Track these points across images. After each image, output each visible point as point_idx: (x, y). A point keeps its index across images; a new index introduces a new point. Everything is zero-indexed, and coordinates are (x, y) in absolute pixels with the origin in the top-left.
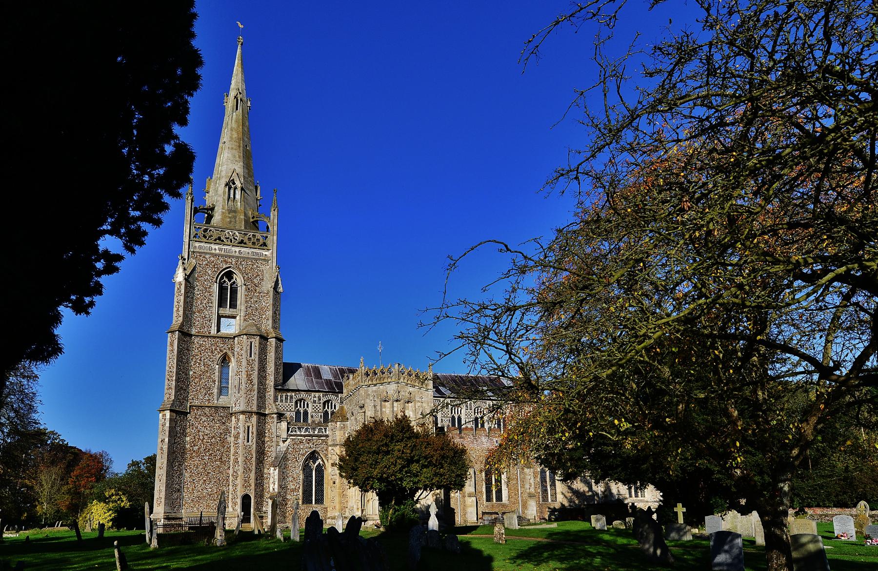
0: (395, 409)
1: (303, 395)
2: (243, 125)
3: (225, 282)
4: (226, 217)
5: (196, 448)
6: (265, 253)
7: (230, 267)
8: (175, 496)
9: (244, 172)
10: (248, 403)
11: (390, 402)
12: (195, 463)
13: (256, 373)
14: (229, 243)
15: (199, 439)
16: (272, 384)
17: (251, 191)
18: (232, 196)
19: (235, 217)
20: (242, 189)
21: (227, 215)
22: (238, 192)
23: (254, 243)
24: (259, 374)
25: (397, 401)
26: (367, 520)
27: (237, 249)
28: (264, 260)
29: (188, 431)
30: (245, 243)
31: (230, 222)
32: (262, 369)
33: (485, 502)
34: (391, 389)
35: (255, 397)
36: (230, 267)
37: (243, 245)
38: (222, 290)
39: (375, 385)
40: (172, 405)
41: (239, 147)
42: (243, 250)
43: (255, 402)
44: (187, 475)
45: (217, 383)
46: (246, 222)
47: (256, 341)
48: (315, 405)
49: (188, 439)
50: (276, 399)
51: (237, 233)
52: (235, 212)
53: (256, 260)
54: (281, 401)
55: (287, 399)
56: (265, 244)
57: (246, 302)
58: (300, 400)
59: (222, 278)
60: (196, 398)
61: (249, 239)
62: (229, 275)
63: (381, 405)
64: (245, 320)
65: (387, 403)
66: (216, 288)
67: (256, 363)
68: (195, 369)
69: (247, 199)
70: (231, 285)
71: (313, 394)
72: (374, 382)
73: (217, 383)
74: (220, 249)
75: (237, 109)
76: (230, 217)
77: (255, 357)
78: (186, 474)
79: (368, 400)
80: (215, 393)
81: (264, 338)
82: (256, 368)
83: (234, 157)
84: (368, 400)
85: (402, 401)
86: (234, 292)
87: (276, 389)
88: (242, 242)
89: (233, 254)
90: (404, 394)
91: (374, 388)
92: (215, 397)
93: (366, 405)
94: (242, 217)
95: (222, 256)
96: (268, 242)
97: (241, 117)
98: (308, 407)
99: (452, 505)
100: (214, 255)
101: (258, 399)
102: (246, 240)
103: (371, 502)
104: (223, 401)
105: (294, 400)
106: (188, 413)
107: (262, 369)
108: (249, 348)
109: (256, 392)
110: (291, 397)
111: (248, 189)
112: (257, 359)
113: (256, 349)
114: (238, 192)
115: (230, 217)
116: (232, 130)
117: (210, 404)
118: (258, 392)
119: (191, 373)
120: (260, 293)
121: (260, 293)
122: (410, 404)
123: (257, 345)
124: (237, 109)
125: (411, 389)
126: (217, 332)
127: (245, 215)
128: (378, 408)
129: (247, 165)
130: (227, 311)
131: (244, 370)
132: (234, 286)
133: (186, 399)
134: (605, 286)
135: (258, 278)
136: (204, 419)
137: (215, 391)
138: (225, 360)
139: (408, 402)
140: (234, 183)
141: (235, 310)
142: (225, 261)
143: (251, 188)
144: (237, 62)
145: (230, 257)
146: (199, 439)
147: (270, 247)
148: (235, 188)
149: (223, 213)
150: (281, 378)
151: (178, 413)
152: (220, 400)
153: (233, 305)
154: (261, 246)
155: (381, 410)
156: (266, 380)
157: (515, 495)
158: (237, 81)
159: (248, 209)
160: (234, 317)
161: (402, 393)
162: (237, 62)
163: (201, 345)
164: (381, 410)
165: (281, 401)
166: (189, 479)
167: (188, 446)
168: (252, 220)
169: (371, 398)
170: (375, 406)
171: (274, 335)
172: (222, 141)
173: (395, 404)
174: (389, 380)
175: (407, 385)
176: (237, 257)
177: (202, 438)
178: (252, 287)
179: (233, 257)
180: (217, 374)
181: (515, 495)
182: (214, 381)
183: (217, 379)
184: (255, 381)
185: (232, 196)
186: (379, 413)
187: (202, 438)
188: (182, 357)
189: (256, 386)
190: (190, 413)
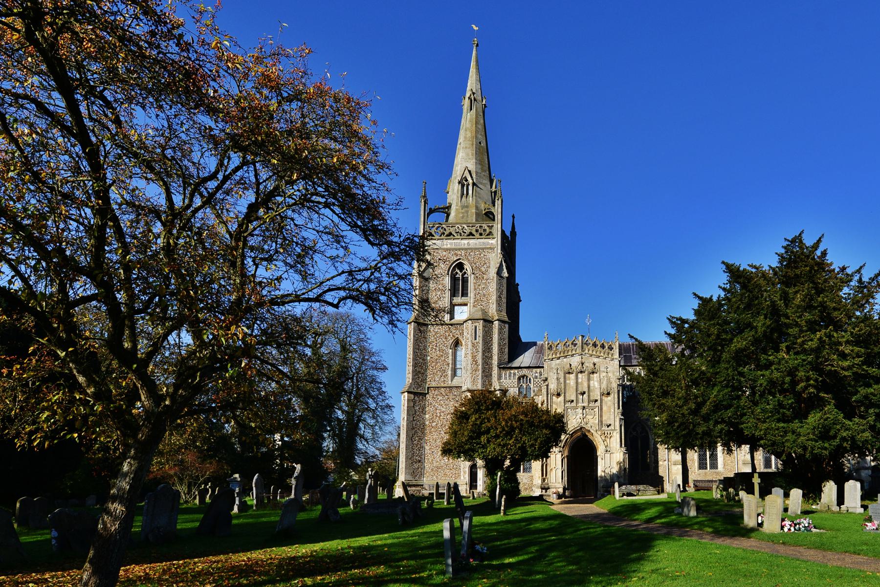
0: (580, 380)
1: (525, 372)
2: (476, 123)
3: (457, 273)
4: (459, 213)
5: (434, 424)
6: (491, 241)
7: (459, 259)
8: (416, 466)
9: (476, 168)
10: (474, 381)
11: (574, 374)
12: (434, 437)
13: (480, 354)
14: (459, 237)
15: (436, 416)
16: (496, 363)
17: (484, 185)
18: (465, 192)
19: (467, 212)
20: (474, 184)
21: (461, 211)
22: (470, 188)
23: (481, 234)
24: (483, 354)
25: (581, 372)
26: (549, 488)
27: (466, 242)
28: (491, 248)
29: (427, 409)
30: (474, 235)
31: (463, 217)
32: (487, 349)
33: (697, 469)
34: (575, 361)
35: (480, 377)
36: (459, 259)
37: (471, 237)
38: (454, 280)
39: (559, 358)
40: (410, 387)
41: (472, 144)
42: (472, 241)
43: (480, 381)
44: (427, 448)
45: (450, 365)
46: (478, 215)
47: (480, 325)
48: (537, 380)
49: (427, 416)
50: (500, 378)
51: (466, 227)
52: (467, 207)
53: (483, 249)
54: (506, 378)
55: (510, 376)
56: (490, 233)
57: (475, 289)
58: (523, 377)
59: (454, 269)
60: (433, 380)
61: (477, 231)
62: (460, 266)
63: (565, 378)
64: (474, 306)
65: (571, 375)
66: (447, 281)
67: (481, 345)
68: (432, 354)
69: (479, 193)
70: (463, 275)
71: (534, 370)
72: (558, 355)
73: (450, 365)
74: (451, 244)
75: (471, 109)
76: (462, 213)
77: (480, 339)
78: (426, 447)
79: (551, 374)
80: (450, 375)
81: (488, 322)
82: (480, 350)
83: (468, 155)
84: (551, 374)
85: (586, 372)
86: (465, 281)
87: (500, 368)
88: (471, 234)
89: (463, 247)
90: (589, 365)
91: (558, 361)
92: (450, 378)
93: (549, 379)
94: (474, 211)
95: (453, 249)
96: (494, 231)
97: (474, 116)
98: (530, 382)
99: (661, 473)
100: (446, 250)
101: (482, 378)
102: (474, 232)
103: (554, 470)
104: (456, 382)
105: (517, 377)
106: (426, 394)
107: (487, 349)
108: (473, 331)
109: (480, 372)
110: (515, 374)
111: (481, 183)
112: (481, 342)
113: (480, 333)
114: (470, 188)
115: (462, 213)
116: (466, 130)
117: (445, 385)
118: (483, 372)
119: (429, 358)
120: (487, 280)
121: (487, 280)
122: (595, 375)
123: (481, 328)
124: (471, 109)
125: (596, 360)
126: (451, 320)
127: (477, 208)
128: (562, 380)
129: (480, 160)
130: (458, 300)
131: (469, 352)
132: (466, 276)
133: (424, 381)
134: (392, 254)
135: (485, 266)
136: (441, 398)
137: (449, 373)
138: (457, 343)
139: (593, 373)
140: (466, 180)
141: (466, 298)
142: (456, 254)
143: (484, 182)
144: (473, 64)
145: (459, 249)
146: (436, 416)
147: (495, 236)
148: (468, 185)
149: (457, 209)
150: (506, 357)
151: (415, 394)
152: (454, 381)
153: (465, 294)
154: (487, 235)
155: (565, 382)
156: (492, 359)
157: (732, 462)
158: (472, 83)
159: (480, 202)
160: (466, 305)
161: (586, 364)
162: (473, 64)
163: (436, 333)
164: (565, 382)
165: (506, 378)
166: (429, 452)
167: (427, 423)
168: (484, 212)
169: (555, 371)
170: (558, 379)
171: (497, 318)
172: (459, 142)
173: (580, 376)
174: (574, 352)
175: (591, 355)
176: (466, 249)
177: (438, 415)
178: (480, 275)
179: (462, 249)
180: (450, 357)
181: (732, 462)
182: (448, 364)
183: (450, 362)
184: (480, 361)
185: (465, 192)
186: (563, 385)
187: (438, 415)
188: (418, 345)
189: (480, 367)
190: (428, 393)
